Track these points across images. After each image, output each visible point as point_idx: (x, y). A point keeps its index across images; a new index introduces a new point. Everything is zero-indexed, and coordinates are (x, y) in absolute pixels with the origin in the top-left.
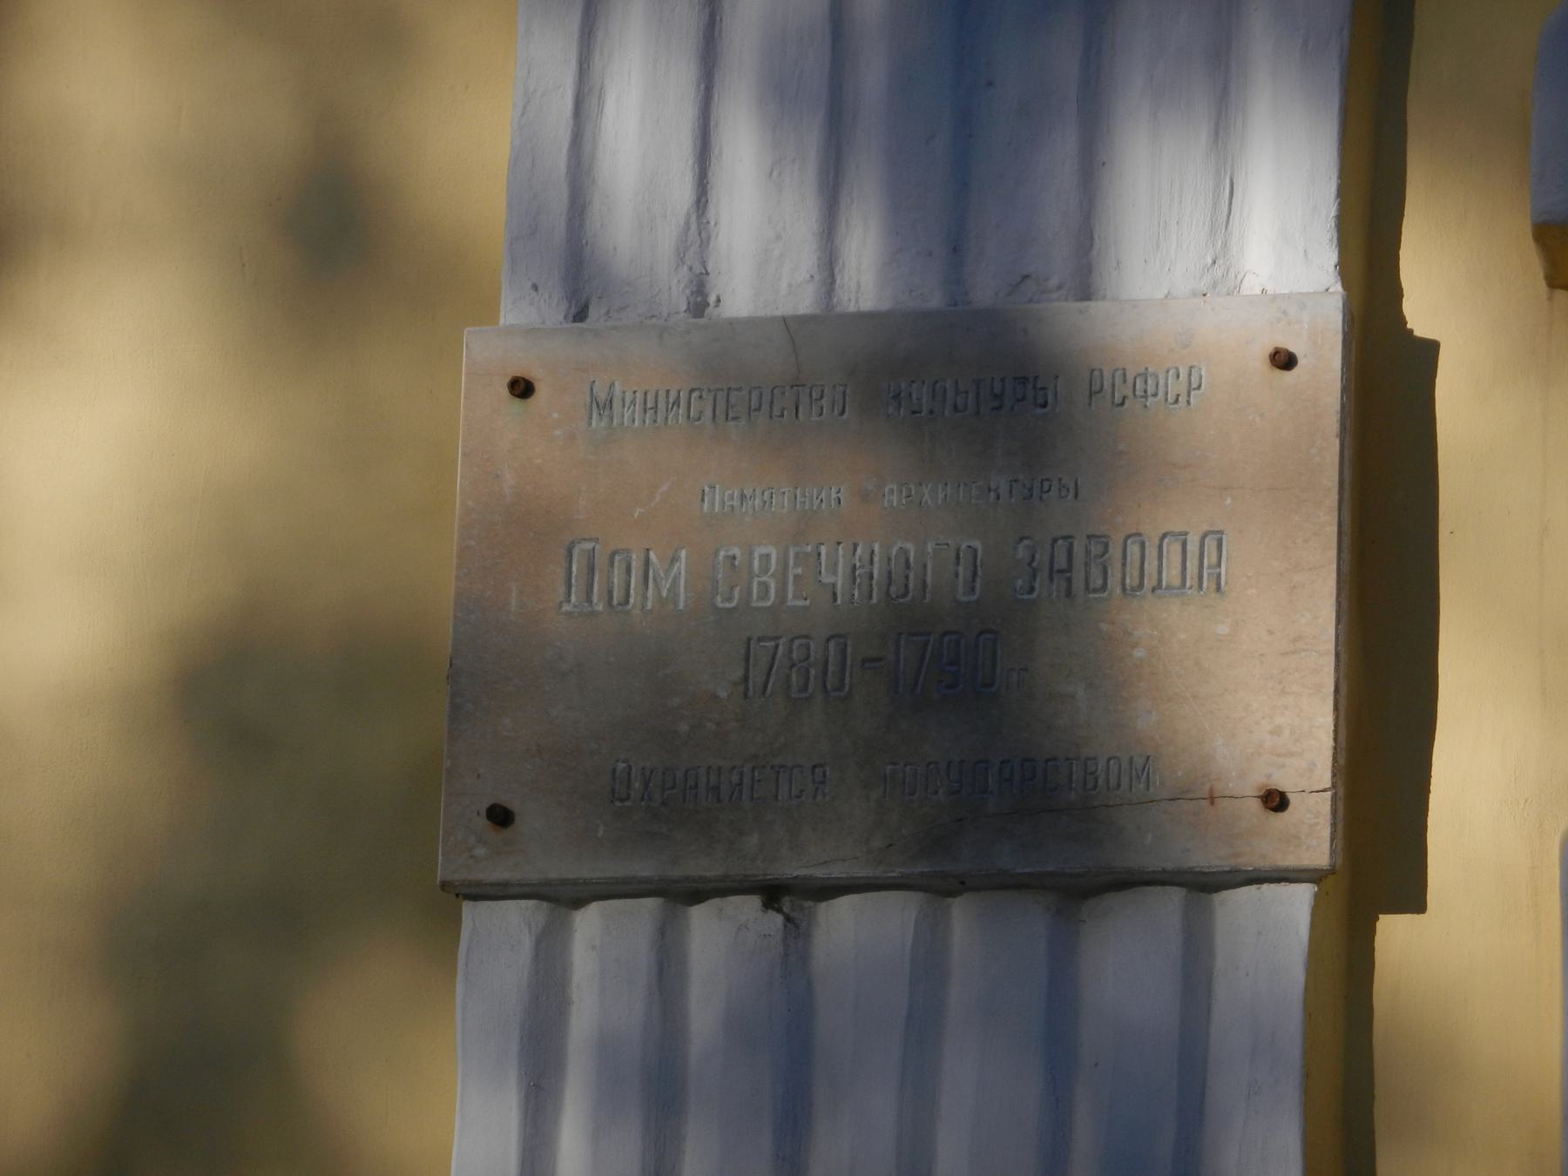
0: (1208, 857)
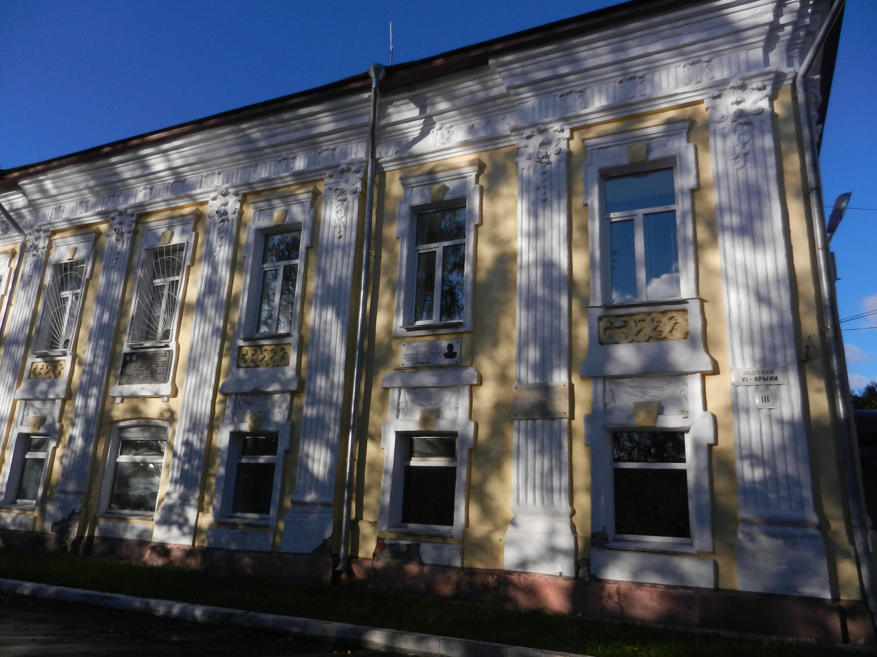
0: (561, 417)
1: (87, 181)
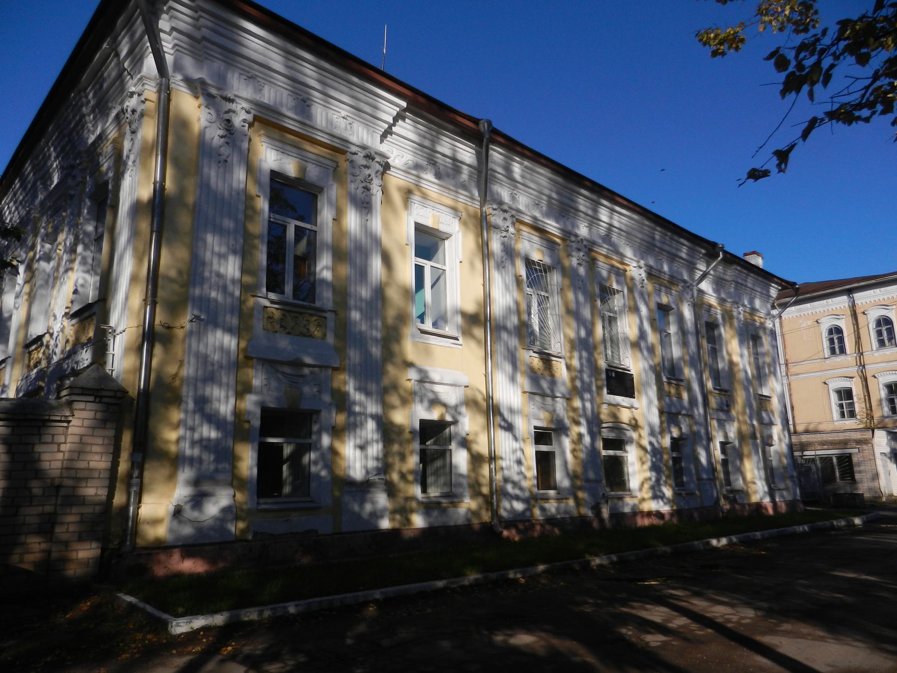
1: (551, 190)
